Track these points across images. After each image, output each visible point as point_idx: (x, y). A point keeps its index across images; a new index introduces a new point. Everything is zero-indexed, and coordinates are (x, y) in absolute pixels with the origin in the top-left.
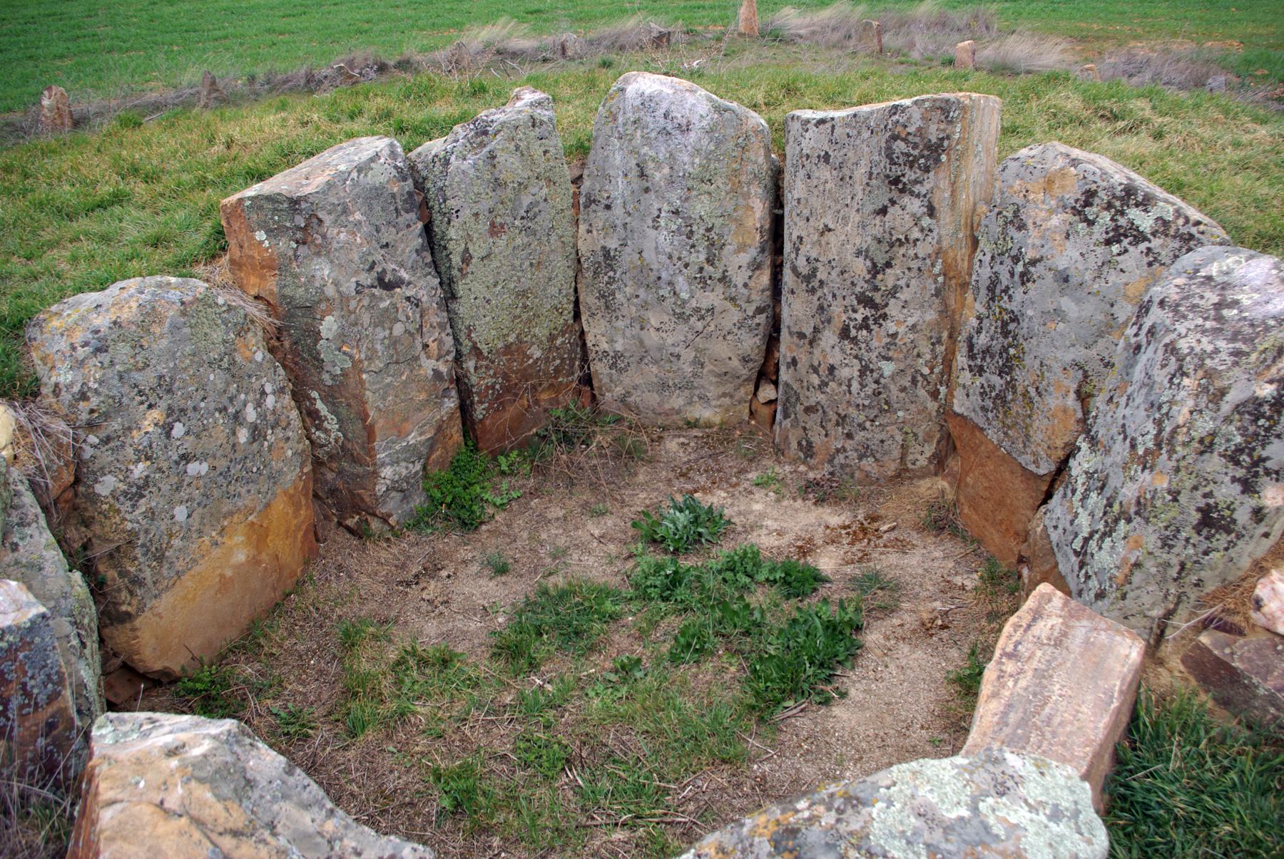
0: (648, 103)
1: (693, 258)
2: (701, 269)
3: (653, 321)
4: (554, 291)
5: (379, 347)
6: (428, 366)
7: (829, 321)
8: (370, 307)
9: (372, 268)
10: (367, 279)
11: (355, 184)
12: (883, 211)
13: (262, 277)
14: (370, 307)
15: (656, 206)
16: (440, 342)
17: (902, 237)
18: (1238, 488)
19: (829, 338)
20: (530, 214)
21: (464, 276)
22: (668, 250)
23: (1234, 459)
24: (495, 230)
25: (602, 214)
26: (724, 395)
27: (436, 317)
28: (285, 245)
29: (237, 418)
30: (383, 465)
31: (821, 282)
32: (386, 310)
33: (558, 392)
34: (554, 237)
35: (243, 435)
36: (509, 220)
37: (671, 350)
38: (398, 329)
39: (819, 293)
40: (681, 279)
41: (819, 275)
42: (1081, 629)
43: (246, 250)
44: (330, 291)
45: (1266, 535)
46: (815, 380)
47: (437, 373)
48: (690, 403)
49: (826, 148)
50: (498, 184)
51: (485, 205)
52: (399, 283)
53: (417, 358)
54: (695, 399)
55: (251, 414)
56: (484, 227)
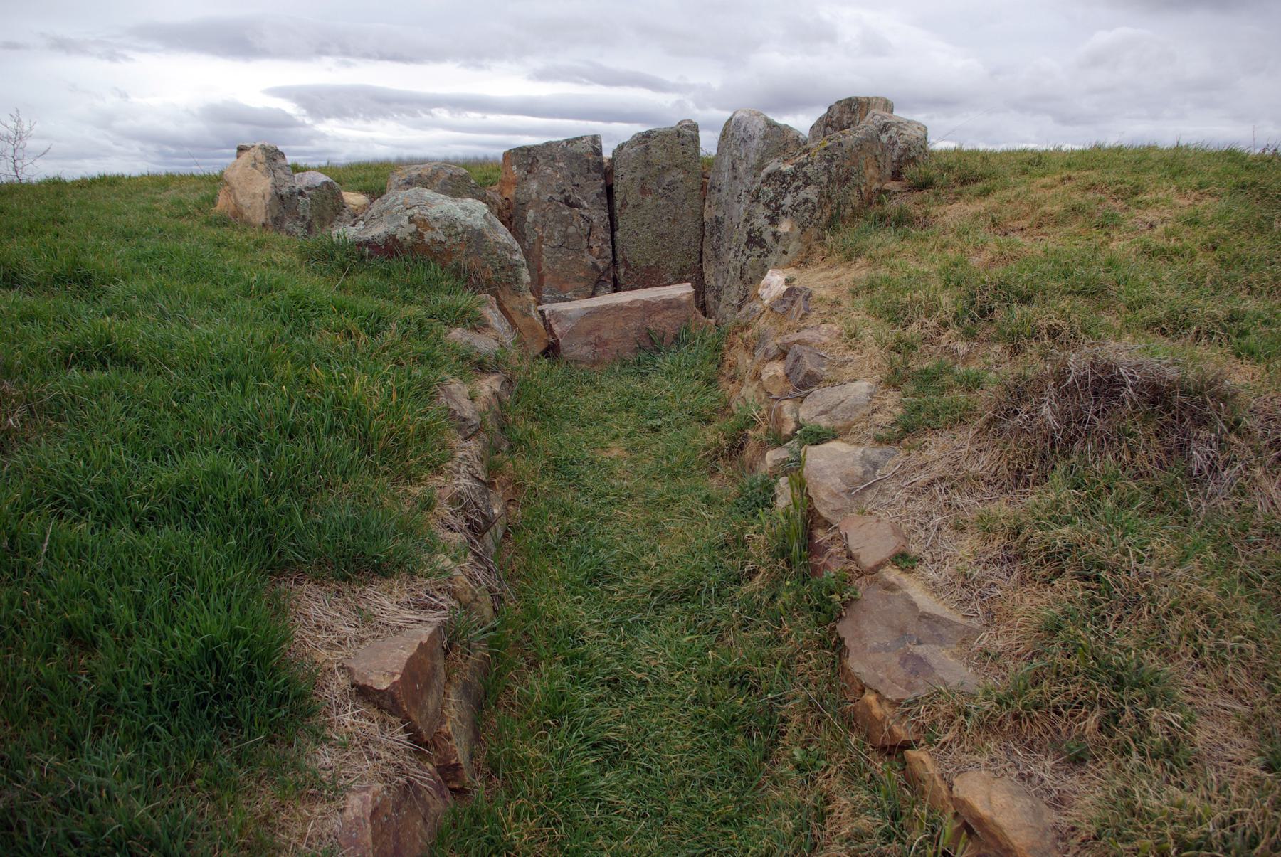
4: (686, 241)
6: (589, 259)
8: (554, 211)
9: (563, 192)
10: (558, 197)
11: (564, 148)
14: (554, 211)
16: (602, 250)
18: (767, 221)
20: (671, 186)
21: (622, 214)
23: (768, 206)
24: (644, 191)
25: (717, 195)
27: (602, 233)
28: (522, 172)
34: (686, 206)
36: (655, 187)
38: (571, 230)
44: (534, 196)
45: (785, 253)
47: (595, 266)
50: (648, 164)
51: (638, 175)
52: (579, 206)
53: (582, 252)
56: (637, 186)
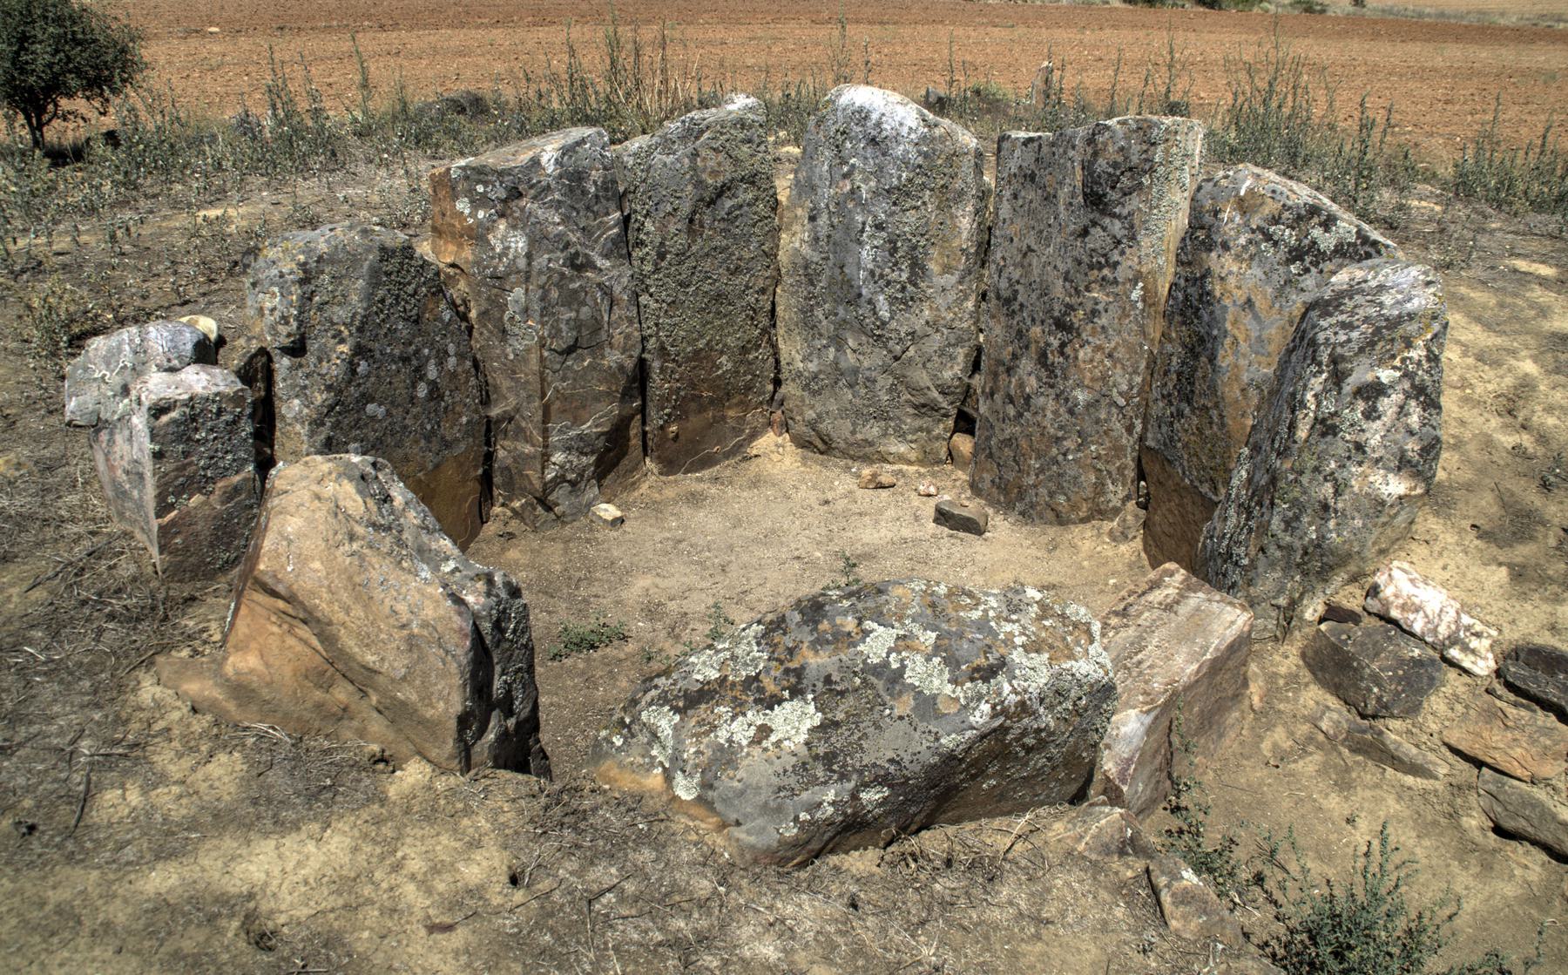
0: (862, 115)
1: (895, 275)
2: (903, 289)
3: (851, 342)
5: (563, 326)
7: (1027, 347)
12: (1085, 233)
13: (460, 246)
15: (859, 218)
17: (1103, 260)
19: (1026, 365)
22: (870, 266)
26: (921, 429)
29: (419, 374)
30: (556, 449)
31: (1022, 305)
32: (575, 291)
33: (746, 411)
35: (422, 391)
37: (868, 373)
39: (1017, 318)
40: (881, 298)
41: (1020, 298)
42: (1197, 599)
43: (448, 219)
46: (1011, 411)
48: (885, 435)
49: (1033, 167)
54: (891, 431)
55: (432, 372)
